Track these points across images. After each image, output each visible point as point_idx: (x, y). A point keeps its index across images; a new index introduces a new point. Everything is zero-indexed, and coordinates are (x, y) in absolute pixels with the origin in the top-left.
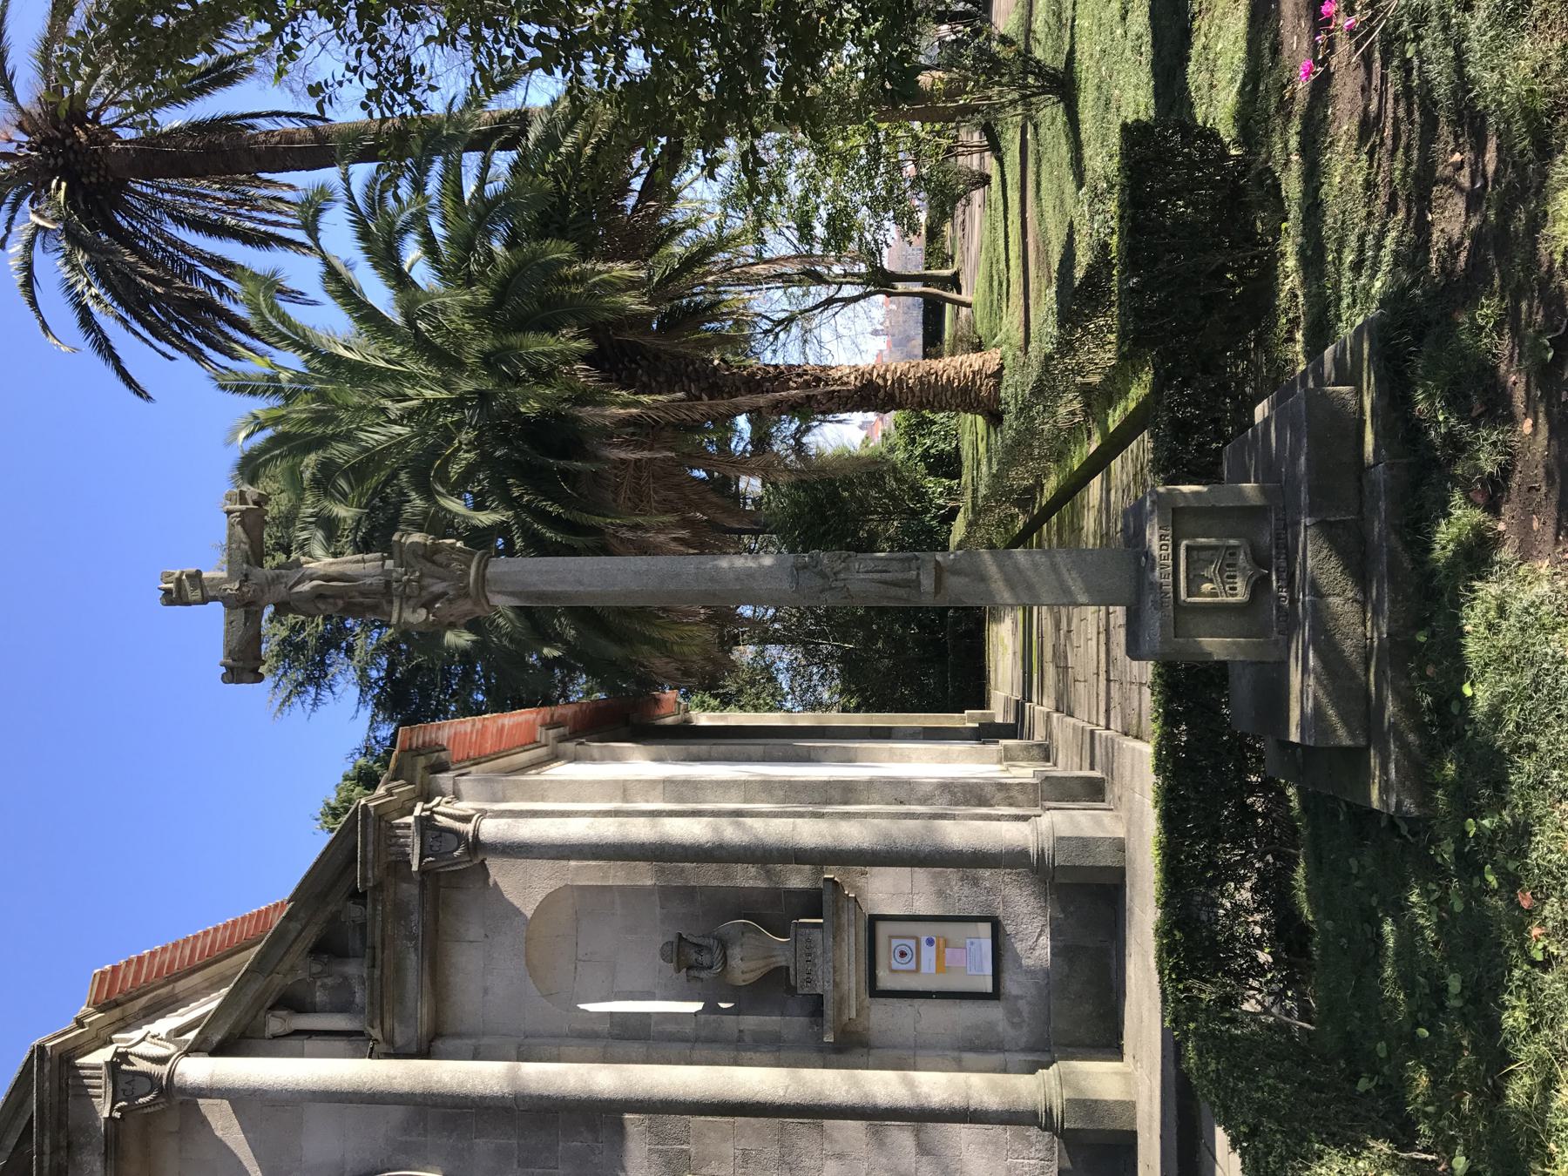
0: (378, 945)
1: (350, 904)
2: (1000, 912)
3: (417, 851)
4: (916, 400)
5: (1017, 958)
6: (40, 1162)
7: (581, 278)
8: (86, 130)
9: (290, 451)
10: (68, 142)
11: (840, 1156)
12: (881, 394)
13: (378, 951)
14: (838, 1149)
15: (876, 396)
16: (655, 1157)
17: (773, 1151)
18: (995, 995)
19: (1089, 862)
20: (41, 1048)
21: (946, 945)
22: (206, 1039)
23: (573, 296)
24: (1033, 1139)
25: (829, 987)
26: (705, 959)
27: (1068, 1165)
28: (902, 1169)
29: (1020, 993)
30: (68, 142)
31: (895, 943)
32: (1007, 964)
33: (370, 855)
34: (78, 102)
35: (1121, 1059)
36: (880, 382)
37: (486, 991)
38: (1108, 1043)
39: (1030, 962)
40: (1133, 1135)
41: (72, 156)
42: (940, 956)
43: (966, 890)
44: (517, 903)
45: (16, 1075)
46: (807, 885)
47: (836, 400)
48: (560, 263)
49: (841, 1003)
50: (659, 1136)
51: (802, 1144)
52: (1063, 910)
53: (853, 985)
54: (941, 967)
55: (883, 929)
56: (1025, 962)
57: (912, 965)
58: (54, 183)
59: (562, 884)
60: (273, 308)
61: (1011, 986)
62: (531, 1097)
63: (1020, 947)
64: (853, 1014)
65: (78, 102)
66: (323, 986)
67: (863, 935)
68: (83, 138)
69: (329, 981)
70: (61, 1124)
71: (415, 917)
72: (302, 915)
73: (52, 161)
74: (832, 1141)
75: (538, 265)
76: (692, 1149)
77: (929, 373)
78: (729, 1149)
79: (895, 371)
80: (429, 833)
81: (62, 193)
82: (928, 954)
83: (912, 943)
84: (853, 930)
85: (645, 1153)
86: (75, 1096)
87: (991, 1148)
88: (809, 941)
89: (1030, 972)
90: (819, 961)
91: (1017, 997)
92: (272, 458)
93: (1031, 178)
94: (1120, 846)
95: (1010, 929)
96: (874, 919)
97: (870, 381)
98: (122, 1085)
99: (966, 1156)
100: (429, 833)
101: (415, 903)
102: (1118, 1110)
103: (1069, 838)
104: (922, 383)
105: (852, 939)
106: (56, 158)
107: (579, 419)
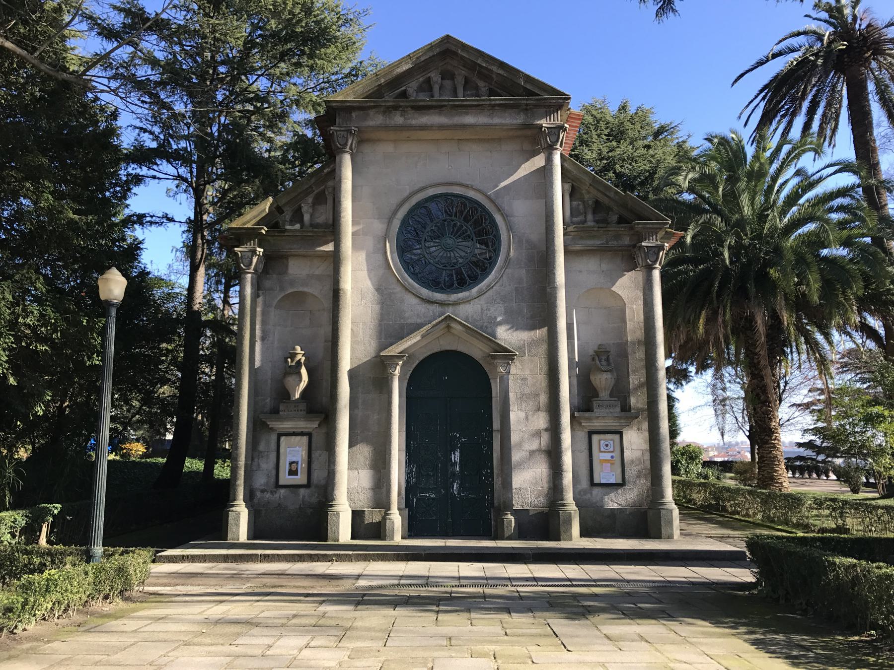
0: (607, 229)
1: (617, 216)
2: (627, 487)
3: (650, 245)
4: (765, 455)
5: (608, 494)
7: (847, 299)
8: (870, 56)
9: (730, 159)
10: (865, 48)
11: (527, 418)
12: (767, 438)
13: (605, 229)
14: (530, 417)
15: (766, 435)
16: (522, 342)
17: (527, 391)
18: (593, 484)
19: (662, 523)
20: (569, 98)
22: (566, 161)
23: (837, 295)
24: (539, 499)
25: (597, 414)
26: (604, 363)
27: (531, 513)
28: (523, 444)
29: (593, 496)
30: (865, 48)
31: (611, 442)
33: (648, 226)
34: (882, 53)
35: (581, 536)
36: (774, 437)
37: (580, 272)
38: (584, 533)
39: (606, 499)
40: (559, 540)
41: (858, 50)
43: (634, 473)
44: (617, 284)
45: (559, 88)
46: (632, 405)
47: (763, 416)
48: (851, 288)
49: (589, 419)
50: (532, 344)
51: (531, 403)
52: (630, 514)
53: (595, 424)
54: (603, 462)
55: (617, 437)
56: (606, 497)
57: (602, 449)
58: (845, 43)
59: (626, 302)
61: (596, 491)
62: (556, 293)
63: (612, 495)
64: (583, 424)
65: (882, 53)
66: (579, 205)
67: (614, 429)
68: (866, 55)
69: (581, 207)
70: (536, 106)
71: (615, 243)
72: (617, 197)
73: (855, 41)
74: (533, 415)
75: (848, 279)
76: (526, 358)
77: (779, 461)
78: (527, 373)
79: (779, 445)
80: (657, 249)
81: (841, 47)
82: (608, 456)
83: (611, 449)
84: (618, 424)
85: (523, 338)
86: (546, 111)
87: (534, 481)
88: (616, 406)
89: (602, 499)
90: (607, 410)
91: (591, 494)
92: (727, 151)
93: (187, 598)
95: (620, 491)
96: (621, 434)
97: (773, 432)
99: (530, 471)
100: (657, 249)
101: (621, 243)
102: (568, 534)
103: (672, 516)
104: (774, 458)
105: (614, 424)
106: (857, 43)
107: (775, 297)
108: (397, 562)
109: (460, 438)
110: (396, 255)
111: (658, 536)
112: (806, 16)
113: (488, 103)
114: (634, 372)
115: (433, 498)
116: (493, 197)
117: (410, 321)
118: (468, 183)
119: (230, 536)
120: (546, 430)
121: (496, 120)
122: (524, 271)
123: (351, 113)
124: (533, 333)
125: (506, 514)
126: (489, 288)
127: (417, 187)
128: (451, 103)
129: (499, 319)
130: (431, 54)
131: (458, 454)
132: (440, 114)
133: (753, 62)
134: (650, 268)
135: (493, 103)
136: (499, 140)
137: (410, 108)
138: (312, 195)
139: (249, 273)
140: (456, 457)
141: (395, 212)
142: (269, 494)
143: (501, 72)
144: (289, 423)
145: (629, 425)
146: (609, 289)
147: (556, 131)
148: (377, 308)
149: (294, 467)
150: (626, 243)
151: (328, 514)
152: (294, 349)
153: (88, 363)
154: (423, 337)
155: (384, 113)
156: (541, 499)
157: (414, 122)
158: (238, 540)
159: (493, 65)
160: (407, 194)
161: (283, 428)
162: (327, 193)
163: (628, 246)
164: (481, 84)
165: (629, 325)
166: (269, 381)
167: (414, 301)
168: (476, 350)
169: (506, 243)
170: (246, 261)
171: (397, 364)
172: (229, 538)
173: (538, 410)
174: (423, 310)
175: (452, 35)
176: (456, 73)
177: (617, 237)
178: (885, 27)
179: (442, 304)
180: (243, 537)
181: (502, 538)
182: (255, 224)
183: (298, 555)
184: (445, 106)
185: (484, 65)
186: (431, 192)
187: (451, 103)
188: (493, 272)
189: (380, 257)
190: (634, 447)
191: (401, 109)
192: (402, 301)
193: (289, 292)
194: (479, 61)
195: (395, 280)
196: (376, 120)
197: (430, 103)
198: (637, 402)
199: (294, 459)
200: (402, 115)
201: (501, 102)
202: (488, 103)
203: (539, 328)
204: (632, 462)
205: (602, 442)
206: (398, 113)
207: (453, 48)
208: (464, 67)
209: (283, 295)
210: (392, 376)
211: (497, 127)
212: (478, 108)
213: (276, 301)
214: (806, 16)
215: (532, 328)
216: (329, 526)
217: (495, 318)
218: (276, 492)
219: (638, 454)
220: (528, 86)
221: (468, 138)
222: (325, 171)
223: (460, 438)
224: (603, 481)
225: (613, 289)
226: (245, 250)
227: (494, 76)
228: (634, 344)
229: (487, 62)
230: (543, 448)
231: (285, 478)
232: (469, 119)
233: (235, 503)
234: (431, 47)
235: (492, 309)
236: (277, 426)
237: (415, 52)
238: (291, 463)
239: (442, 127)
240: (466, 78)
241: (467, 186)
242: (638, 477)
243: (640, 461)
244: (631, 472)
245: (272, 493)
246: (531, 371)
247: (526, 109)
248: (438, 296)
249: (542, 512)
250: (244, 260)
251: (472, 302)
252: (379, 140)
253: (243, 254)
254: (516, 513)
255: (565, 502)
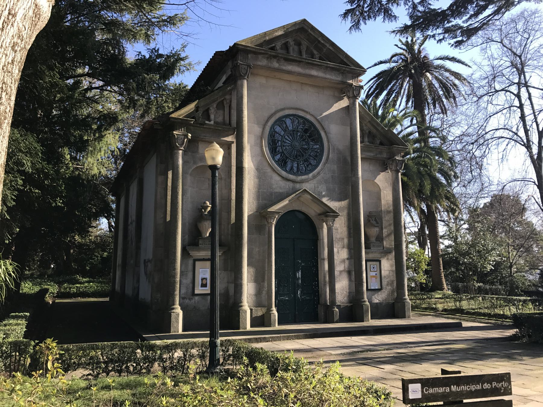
1: (380, 141)
2: (383, 291)
5: (374, 295)
6: (344, 67)
21: (376, 278)
25: (373, 251)
27: (342, 307)
32: (373, 292)
38: (251, 327)
42: (374, 276)
44: (377, 178)
53: (370, 256)
55: (378, 263)
57: (372, 270)
60: (409, 116)
63: (376, 295)
74: (341, 250)
83: (376, 270)
90: (377, 248)
94: (409, 317)
95: (379, 293)
98: (357, 88)
108: (306, 340)
109: (301, 263)
110: (267, 148)
111: (270, 326)
112: (396, 45)
113: (326, 65)
114: (385, 228)
115: (287, 300)
116: (320, 120)
117: (276, 191)
118: (307, 110)
119: (172, 330)
120: (348, 259)
121: (328, 76)
122: (336, 167)
123: (248, 54)
124: (340, 203)
125: (334, 308)
126: (318, 173)
127: (279, 108)
128: (307, 61)
129: (323, 193)
130: (294, 28)
131: (300, 273)
132: (298, 66)
133: (373, 64)
134: (398, 171)
135: (329, 65)
136: (323, 88)
137: (283, 59)
138: (216, 102)
139: (181, 150)
140: (299, 275)
141: (267, 121)
142: (188, 300)
143: (331, 48)
144: (204, 252)
145: (383, 257)
146: (373, 181)
147: (358, 88)
148: (257, 180)
149: (204, 282)
150: (385, 156)
151: (240, 312)
152: (205, 203)
153: (54, 205)
154: (289, 201)
155: (268, 58)
156: (346, 299)
157: (284, 68)
158: (246, 329)
159: (327, 43)
160: (273, 111)
161: (198, 256)
162: (225, 103)
163: (385, 158)
164: (315, 52)
165: (383, 202)
166: (187, 224)
167: (278, 178)
168: (312, 211)
169: (327, 149)
170: (180, 141)
171: (275, 217)
172: (171, 331)
173: (343, 247)
174: (283, 185)
175: (307, 20)
176: (302, 43)
177: (381, 153)
178: (436, 59)
179: (294, 182)
180: (180, 331)
181: (332, 322)
182: (185, 117)
183: (248, 339)
184: (302, 62)
185: (322, 42)
186: (287, 112)
187: (307, 61)
188: (320, 165)
189: (258, 149)
190: (386, 269)
191: (277, 58)
192: (271, 178)
193: (199, 165)
194: (320, 39)
195: (266, 164)
196: (263, 62)
197: (295, 58)
198: (387, 244)
199: (204, 276)
200: (277, 62)
201: (333, 66)
202: (326, 65)
203: (344, 200)
204: (385, 277)
205: (371, 266)
206: (275, 60)
207: (306, 28)
208: (307, 40)
209: (195, 166)
210: (272, 223)
211: (328, 80)
212: (319, 67)
213: (191, 170)
214: (396, 45)
215: (340, 200)
216: (240, 319)
217: (322, 193)
218: (192, 299)
219: (387, 273)
220: (345, 60)
221: (307, 83)
222: (228, 89)
223: (301, 263)
224: (372, 288)
225: (375, 181)
226: (180, 133)
227: (325, 50)
228: (385, 212)
229: (324, 40)
230: (346, 269)
231: (199, 290)
232: (314, 72)
233: (174, 307)
234: (295, 24)
235: (320, 187)
236: (195, 254)
237: (287, 25)
238: (202, 279)
239: (299, 74)
240: (307, 47)
241: (306, 112)
242: (387, 285)
243: (388, 276)
244: (384, 283)
245: (190, 299)
246: (340, 225)
247: (342, 73)
248: (291, 177)
249: (347, 306)
250: (178, 140)
251: (309, 182)
252: (257, 75)
253: (179, 136)
254: (338, 307)
255: (242, 304)
